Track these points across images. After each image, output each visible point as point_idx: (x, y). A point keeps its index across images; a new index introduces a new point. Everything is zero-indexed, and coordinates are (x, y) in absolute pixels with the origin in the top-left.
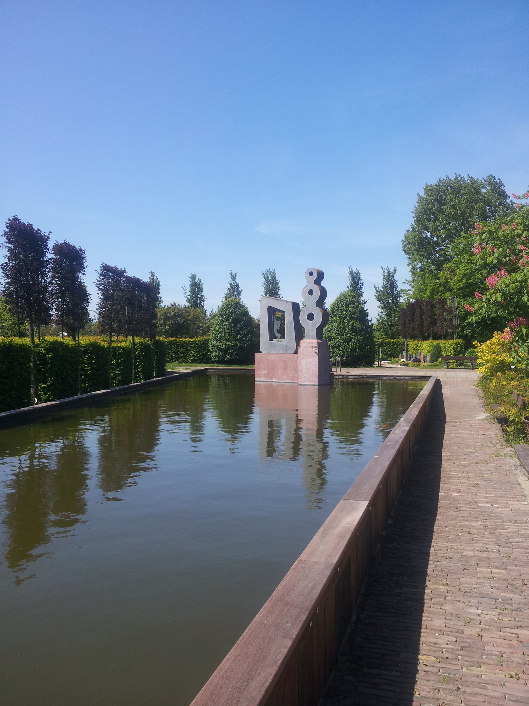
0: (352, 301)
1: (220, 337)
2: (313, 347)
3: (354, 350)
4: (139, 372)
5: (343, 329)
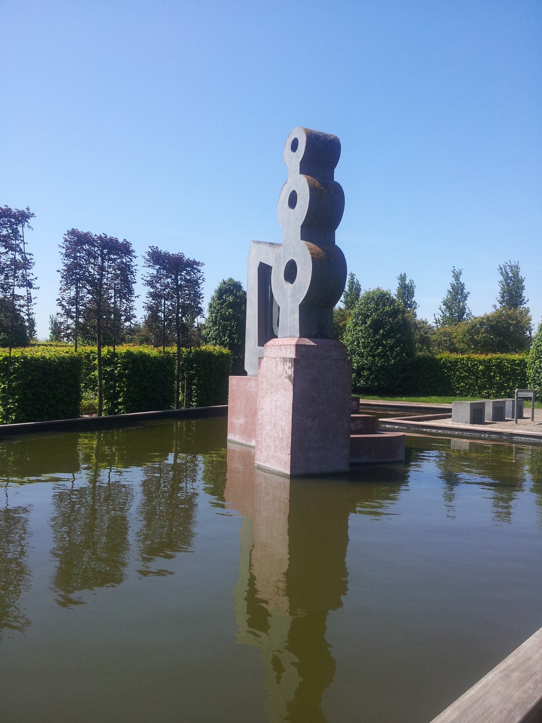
1: (351, 350)
2: (285, 360)
4: (120, 404)
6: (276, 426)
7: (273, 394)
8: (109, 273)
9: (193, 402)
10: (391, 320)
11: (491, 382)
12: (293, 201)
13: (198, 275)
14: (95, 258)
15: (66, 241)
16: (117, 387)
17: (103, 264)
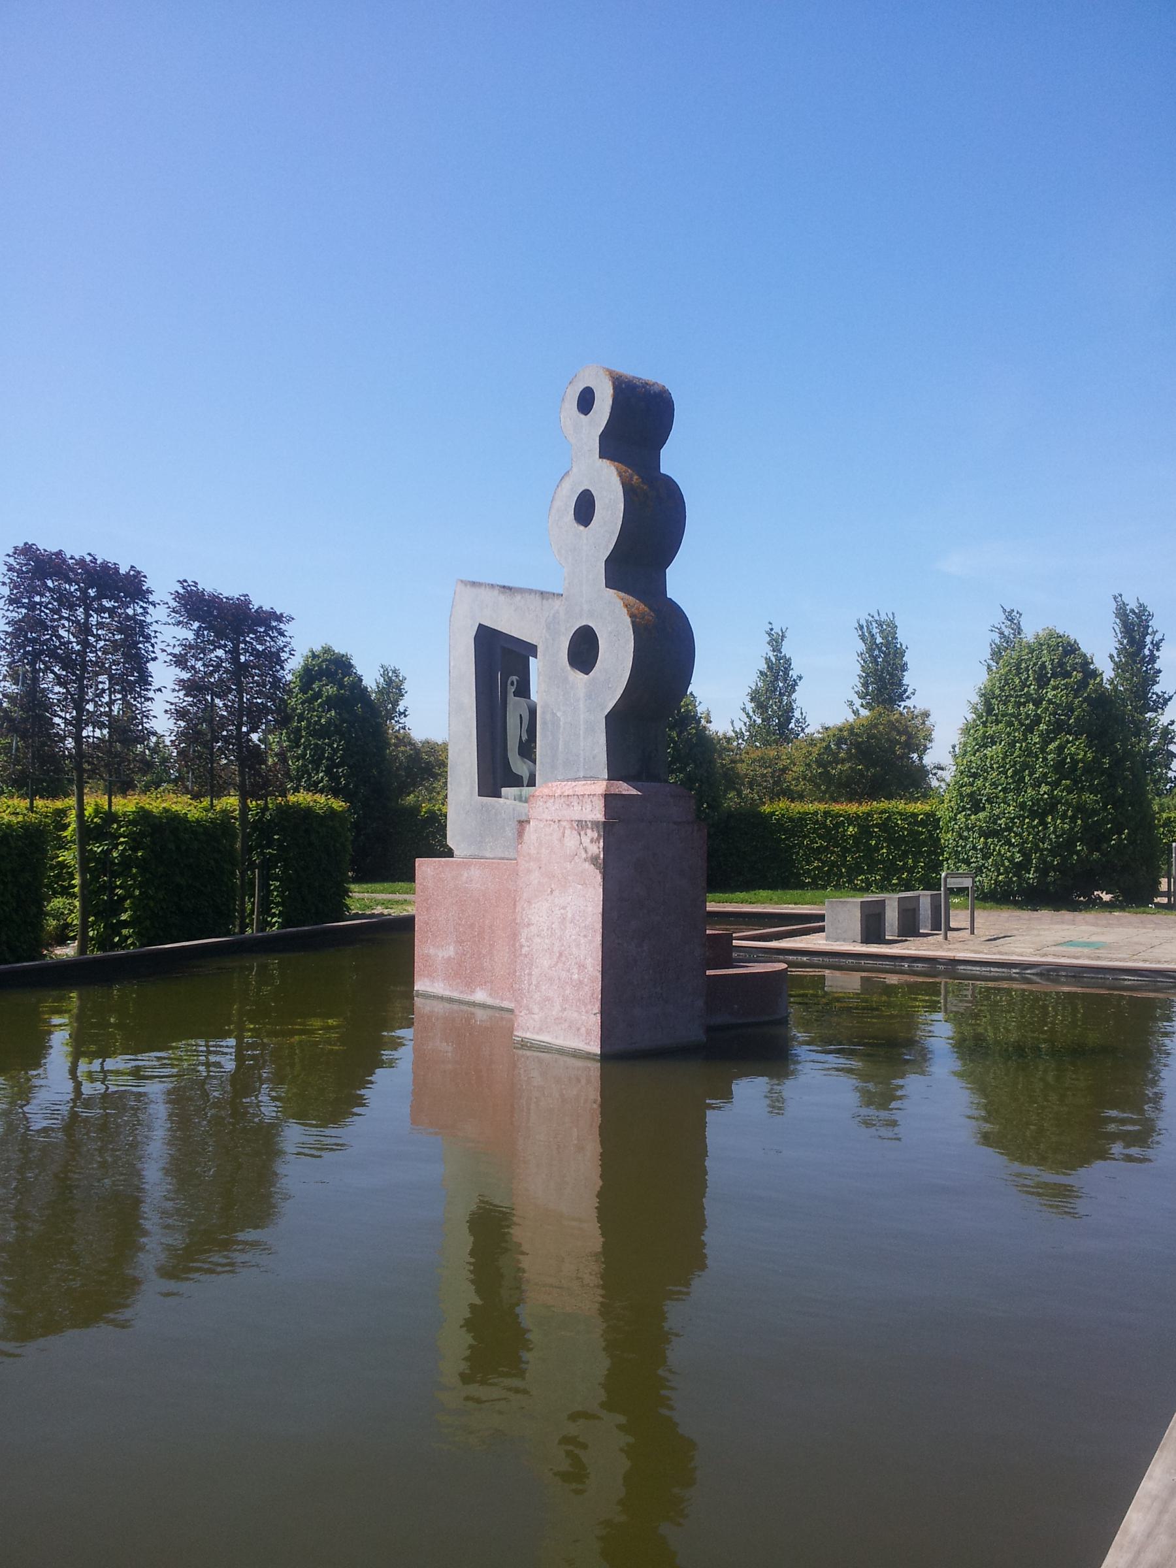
0: (1061, 664)
2: (581, 825)
3: (1066, 845)
4: (125, 924)
5: (1025, 766)
6: (563, 959)
7: (556, 893)
8: (98, 638)
9: (274, 915)
10: (674, 734)
11: (872, 859)
12: (585, 509)
13: (281, 641)
14: (72, 607)
15: (11, 569)
16: (117, 887)
17: (87, 619)
